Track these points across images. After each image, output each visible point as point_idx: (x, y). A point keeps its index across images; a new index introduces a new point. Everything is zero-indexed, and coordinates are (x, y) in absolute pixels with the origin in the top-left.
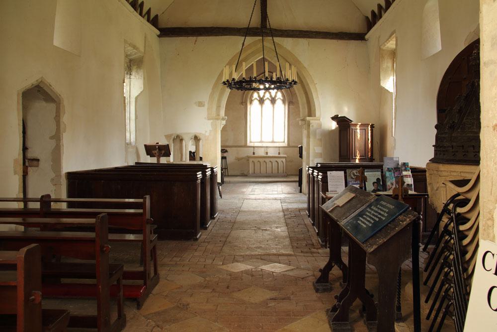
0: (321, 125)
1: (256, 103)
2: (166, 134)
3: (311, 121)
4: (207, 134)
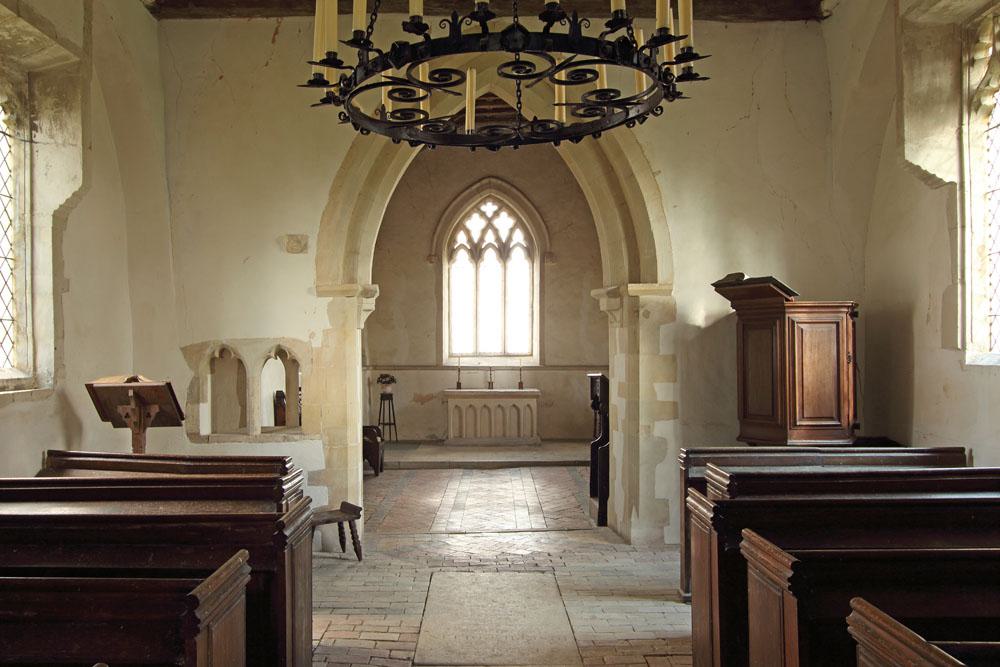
0: (675, 310)
1: (462, 256)
2: (182, 346)
3: (643, 298)
4: (317, 343)
